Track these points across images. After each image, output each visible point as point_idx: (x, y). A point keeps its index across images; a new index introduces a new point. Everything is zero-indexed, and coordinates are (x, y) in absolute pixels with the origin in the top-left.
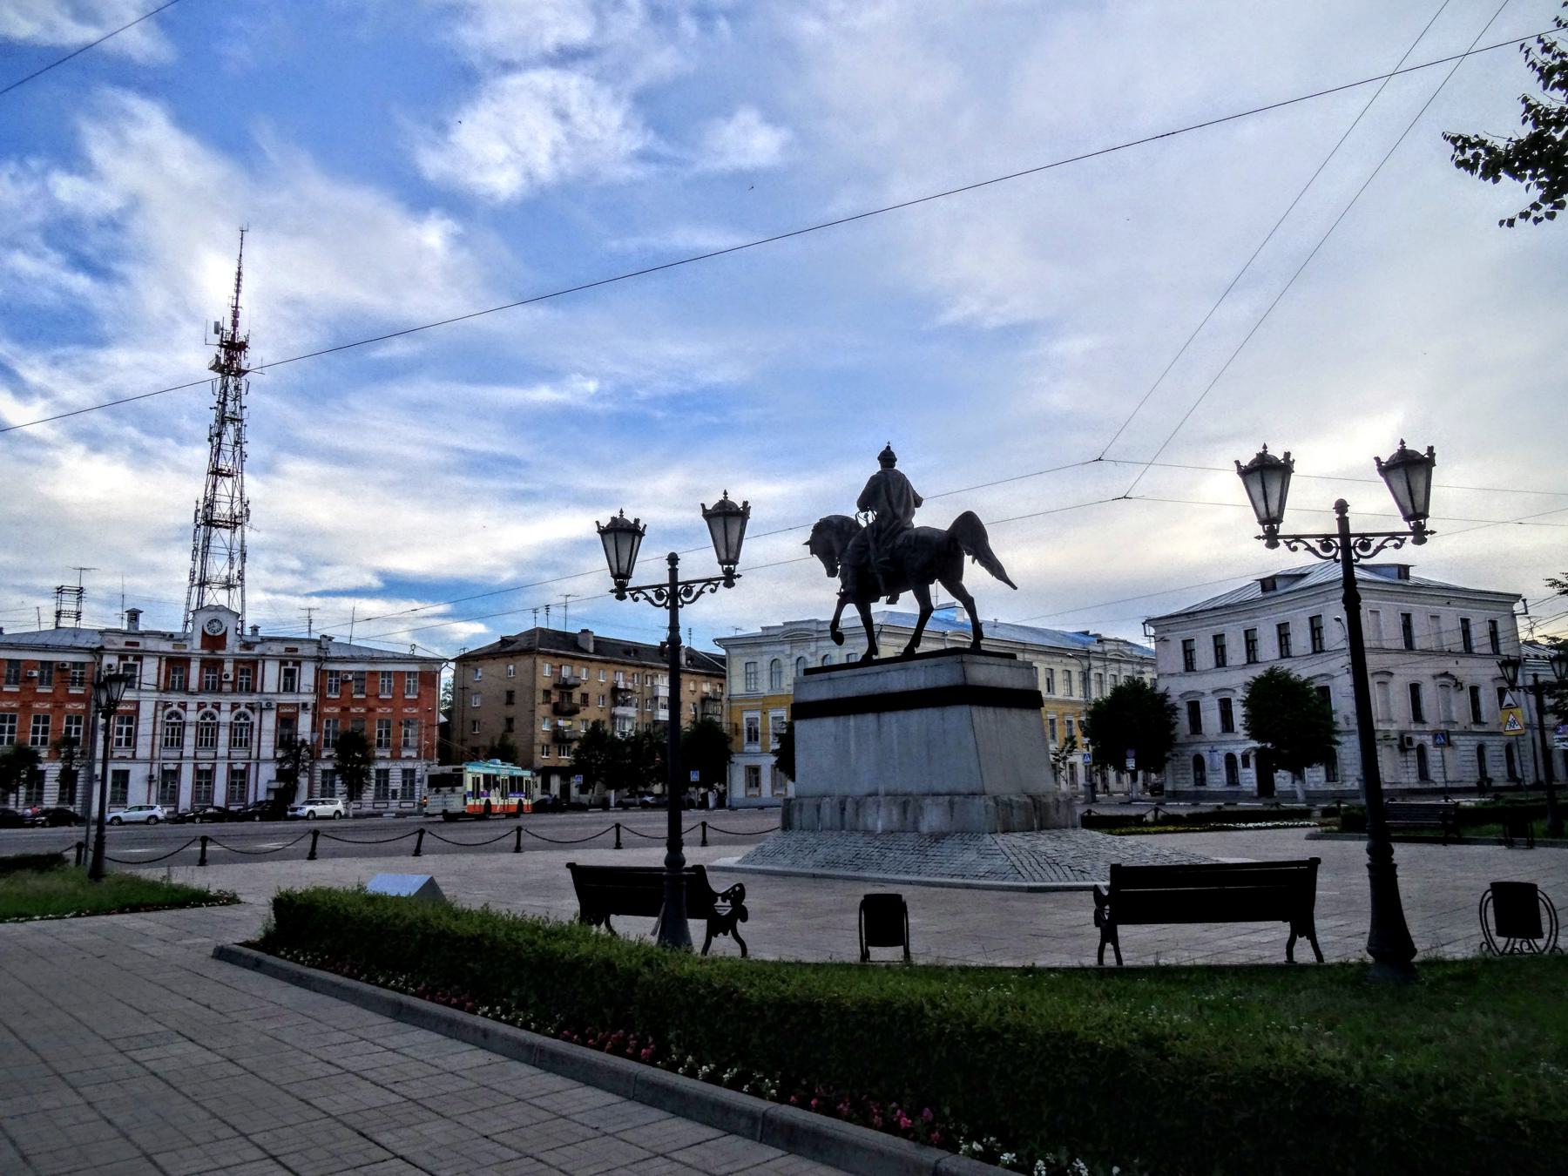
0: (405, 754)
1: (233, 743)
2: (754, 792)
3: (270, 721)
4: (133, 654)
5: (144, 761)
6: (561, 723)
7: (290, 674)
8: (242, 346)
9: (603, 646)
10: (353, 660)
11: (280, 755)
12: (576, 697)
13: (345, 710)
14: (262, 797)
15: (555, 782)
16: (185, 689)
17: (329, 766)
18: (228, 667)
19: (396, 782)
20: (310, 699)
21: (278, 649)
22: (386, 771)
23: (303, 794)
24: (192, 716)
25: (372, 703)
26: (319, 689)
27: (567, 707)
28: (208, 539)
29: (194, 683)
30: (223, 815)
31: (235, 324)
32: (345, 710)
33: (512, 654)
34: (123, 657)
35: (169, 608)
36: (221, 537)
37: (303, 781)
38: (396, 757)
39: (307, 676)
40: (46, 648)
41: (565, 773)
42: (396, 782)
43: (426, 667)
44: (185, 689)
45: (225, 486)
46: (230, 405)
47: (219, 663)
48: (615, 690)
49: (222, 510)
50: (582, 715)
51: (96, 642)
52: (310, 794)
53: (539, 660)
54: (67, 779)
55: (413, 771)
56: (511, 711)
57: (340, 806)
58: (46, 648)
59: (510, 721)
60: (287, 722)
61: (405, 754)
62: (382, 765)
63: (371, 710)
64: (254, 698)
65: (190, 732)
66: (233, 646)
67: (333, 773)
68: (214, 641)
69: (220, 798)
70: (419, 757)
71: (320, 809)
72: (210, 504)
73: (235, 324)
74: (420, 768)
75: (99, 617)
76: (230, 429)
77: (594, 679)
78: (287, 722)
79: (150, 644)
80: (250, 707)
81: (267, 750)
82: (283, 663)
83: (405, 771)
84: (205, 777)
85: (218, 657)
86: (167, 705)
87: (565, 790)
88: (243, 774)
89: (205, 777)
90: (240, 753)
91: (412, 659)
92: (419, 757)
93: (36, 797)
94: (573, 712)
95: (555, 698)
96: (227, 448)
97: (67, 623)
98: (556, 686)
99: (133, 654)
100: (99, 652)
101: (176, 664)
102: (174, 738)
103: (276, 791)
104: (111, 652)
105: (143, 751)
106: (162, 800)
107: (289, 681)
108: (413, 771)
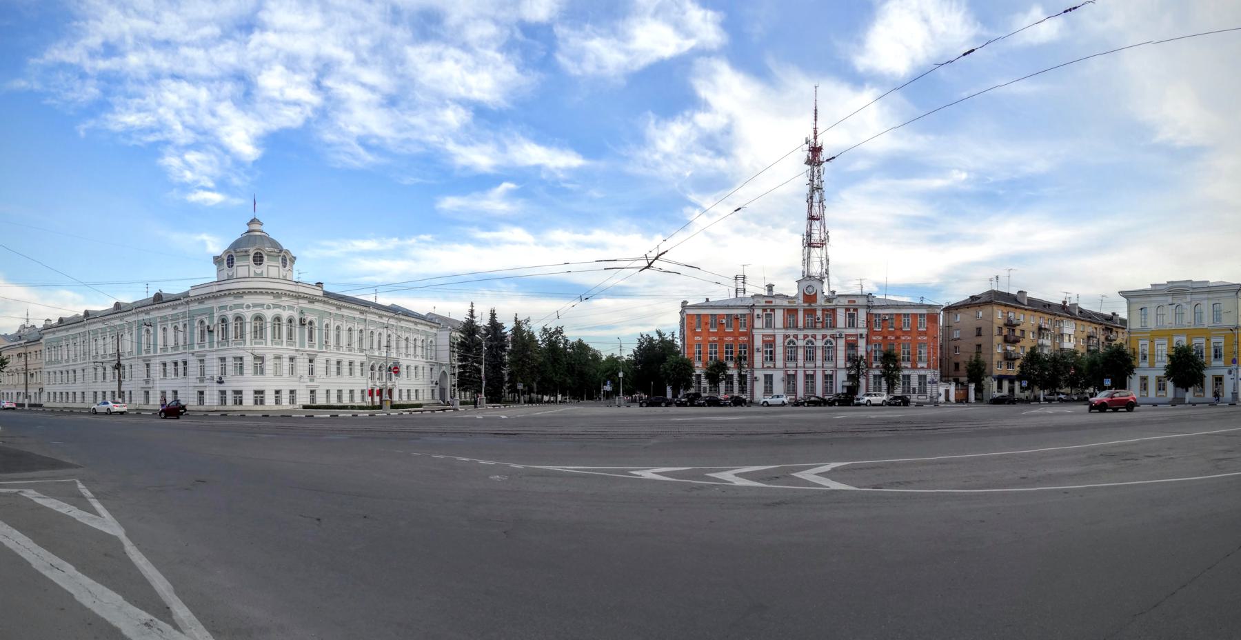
0: (919, 365)
1: (824, 359)
2: (1162, 393)
3: (841, 344)
4: (769, 310)
5: (780, 369)
6: (1009, 348)
7: (852, 316)
8: (820, 149)
9: (1032, 302)
10: (887, 307)
11: (848, 365)
12: (1018, 333)
13: (885, 338)
14: (839, 391)
15: (1006, 384)
16: (796, 327)
17: (877, 372)
18: (819, 313)
19: (915, 383)
20: (864, 331)
21: (845, 301)
22: (909, 376)
23: (862, 390)
24: (801, 343)
25: (898, 333)
26: (869, 322)
27: (1012, 338)
28: (809, 253)
29: (801, 324)
30: (821, 402)
31: (815, 138)
32: (885, 338)
33: (980, 305)
34: (764, 310)
35: (789, 287)
36: (816, 252)
37: (863, 381)
38: (914, 367)
39: (862, 315)
40: (728, 307)
41: (1011, 380)
42: (915, 383)
43: (931, 311)
44: (796, 327)
45: (816, 224)
46: (816, 182)
47: (815, 311)
48: (1040, 329)
49: (816, 237)
50: (1021, 344)
51: (750, 303)
52: (867, 390)
53: (995, 308)
54: (742, 378)
55: (925, 376)
56: (979, 340)
57: (884, 398)
58: (728, 307)
59: (979, 346)
60: (852, 346)
61: (919, 365)
62: (906, 372)
63: (898, 338)
64: (834, 332)
65: (801, 352)
66: (821, 301)
67: (880, 377)
68: (810, 298)
69: (801, 393)
70: (929, 367)
71: (874, 399)
72: (809, 235)
73: (815, 138)
74: (930, 374)
75: (755, 287)
76: (817, 194)
77: (1027, 321)
78: (852, 346)
79: (777, 302)
80: (833, 336)
81: (841, 362)
82: (847, 310)
83: (920, 376)
84: (810, 378)
85: (813, 307)
86: (787, 336)
87: (1011, 390)
88: (831, 376)
89: (810, 378)
90: (828, 365)
91: (921, 306)
92: (929, 367)
93: (729, 389)
94: (1016, 341)
95: (1005, 331)
96: (816, 205)
97: (741, 295)
98: (1006, 325)
99: (769, 310)
100: (752, 307)
101: (791, 312)
102: (791, 357)
103: (848, 387)
104: (759, 307)
105: (779, 363)
106: (788, 392)
107: (852, 322)
108: (925, 376)
